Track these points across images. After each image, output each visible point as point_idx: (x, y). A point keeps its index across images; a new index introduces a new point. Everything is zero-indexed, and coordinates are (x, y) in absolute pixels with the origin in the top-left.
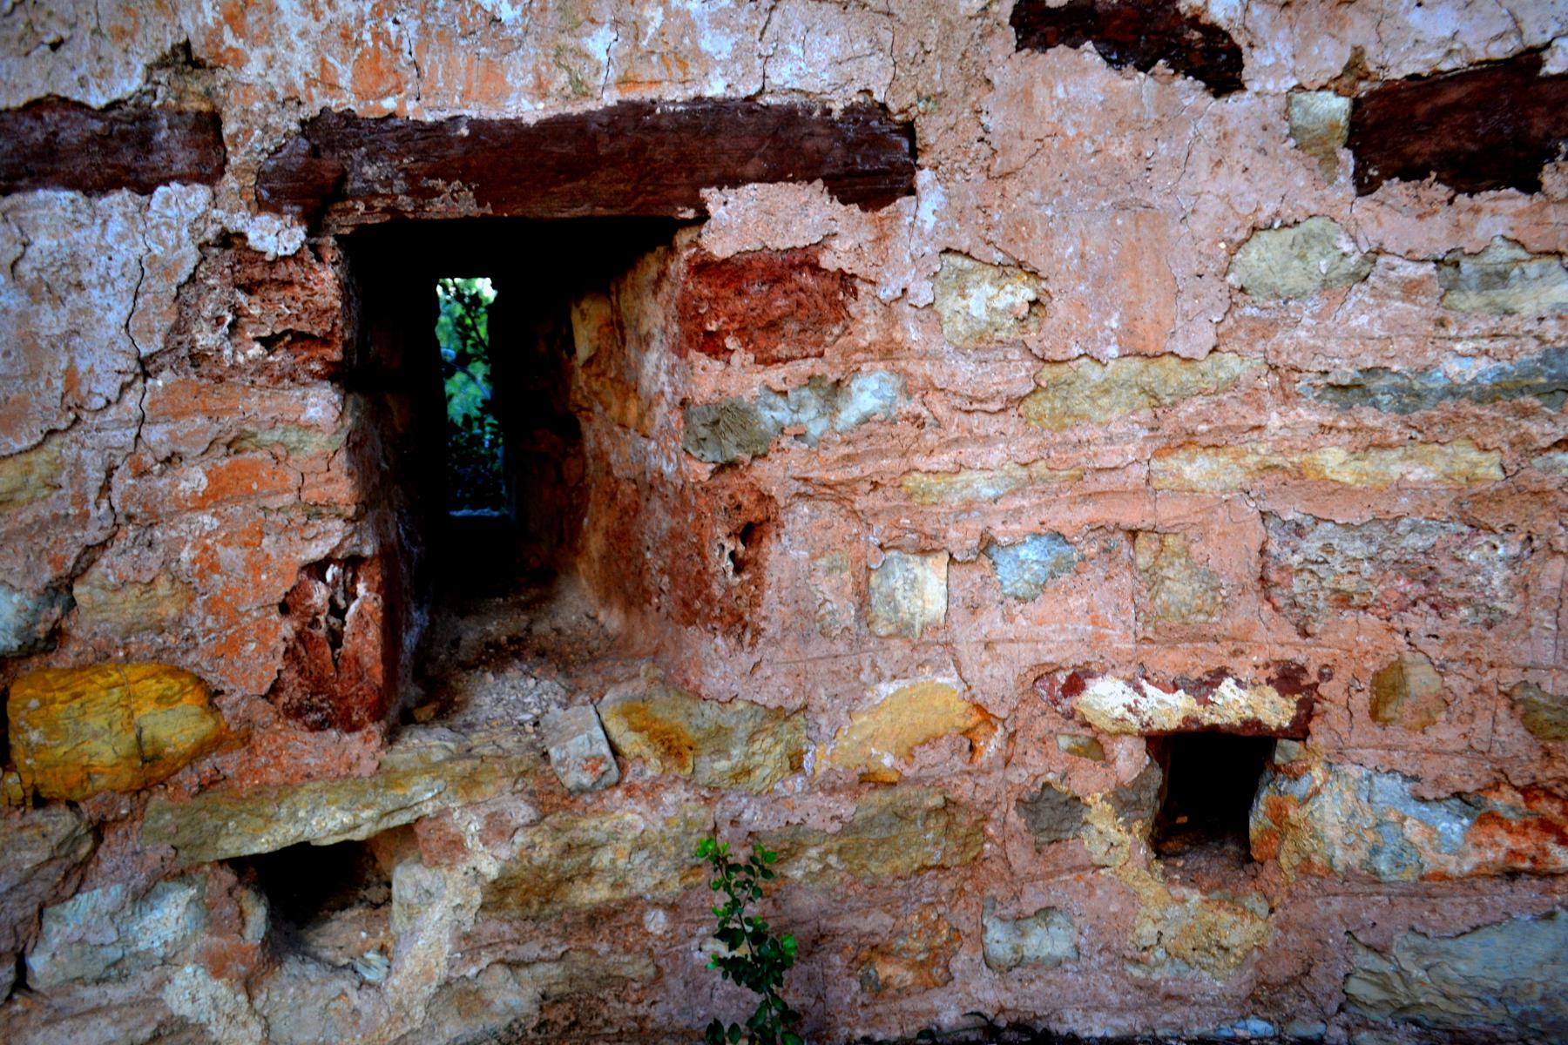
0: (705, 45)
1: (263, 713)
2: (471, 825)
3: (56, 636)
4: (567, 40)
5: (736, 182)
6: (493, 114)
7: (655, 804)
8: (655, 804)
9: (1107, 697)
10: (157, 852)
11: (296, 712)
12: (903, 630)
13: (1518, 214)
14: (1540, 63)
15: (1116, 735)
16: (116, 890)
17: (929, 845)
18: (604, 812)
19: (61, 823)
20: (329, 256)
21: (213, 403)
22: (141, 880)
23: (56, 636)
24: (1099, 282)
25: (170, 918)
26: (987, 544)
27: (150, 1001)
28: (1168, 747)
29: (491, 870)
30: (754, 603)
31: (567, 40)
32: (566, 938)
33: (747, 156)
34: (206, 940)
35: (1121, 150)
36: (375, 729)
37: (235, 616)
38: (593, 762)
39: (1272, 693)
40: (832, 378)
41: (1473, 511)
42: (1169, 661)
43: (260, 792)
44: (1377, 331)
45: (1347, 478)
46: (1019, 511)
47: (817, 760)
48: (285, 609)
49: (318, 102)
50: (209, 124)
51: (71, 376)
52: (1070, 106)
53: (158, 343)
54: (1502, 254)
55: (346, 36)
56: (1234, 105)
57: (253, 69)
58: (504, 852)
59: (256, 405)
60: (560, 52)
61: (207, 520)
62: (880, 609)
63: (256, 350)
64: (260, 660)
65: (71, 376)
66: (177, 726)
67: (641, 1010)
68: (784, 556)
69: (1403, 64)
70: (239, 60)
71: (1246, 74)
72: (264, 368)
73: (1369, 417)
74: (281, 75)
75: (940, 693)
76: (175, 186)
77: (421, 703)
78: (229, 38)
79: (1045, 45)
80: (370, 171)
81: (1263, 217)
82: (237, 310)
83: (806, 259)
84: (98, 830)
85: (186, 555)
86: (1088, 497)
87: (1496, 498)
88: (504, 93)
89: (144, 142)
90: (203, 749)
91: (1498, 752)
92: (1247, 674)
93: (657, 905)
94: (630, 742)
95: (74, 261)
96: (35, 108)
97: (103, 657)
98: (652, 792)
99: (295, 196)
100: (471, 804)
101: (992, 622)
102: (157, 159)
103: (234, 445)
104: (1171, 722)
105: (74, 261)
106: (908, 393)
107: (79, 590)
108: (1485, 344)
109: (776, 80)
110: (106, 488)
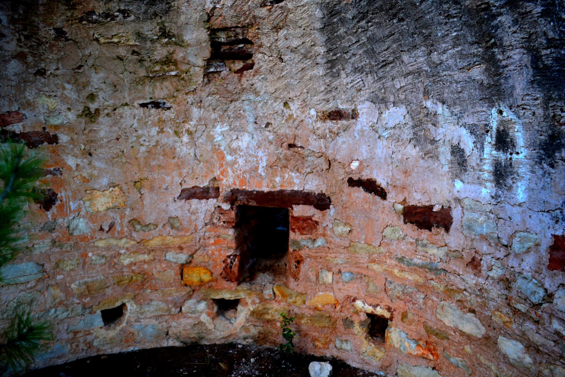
0: (295, 181)
1: (219, 277)
2: (249, 301)
3: (190, 262)
4: (272, 179)
5: (298, 204)
6: (260, 190)
7: (280, 304)
8: (280, 304)
9: (359, 304)
10: (202, 296)
11: (224, 278)
12: (324, 284)
13: (428, 235)
14: (432, 208)
15: (361, 311)
16: (195, 300)
17: (325, 323)
18: (270, 304)
19: (188, 289)
20: (234, 209)
21: (215, 230)
22: (199, 299)
23: (190, 262)
24: (362, 229)
25: (202, 306)
26: (340, 272)
27: (198, 318)
28: (371, 316)
29: (252, 309)
30: (298, 274)
31: (272, 179)
32: (263, 323)
33: (300, 200)
34: (207, 310)
35: (366, 206)
36: (236, 283)
37: (216, 262)
38: (270, 295)
39: (386, 311)
40: (313, 238)
41: (418, 287)
42: (370, 300)
43: (217, 289)
44: (405, 250)
45: (398, 275)
46: (346, 267)
47: (307, 303)
48: (224, 262)
49: (233, 187)
50: (218, 189)
51: (196, 225)
52: (358, 197)
53: (208, 221)
54: (425, 242)
55: (238, 177)
56: (385, 202)
57: (224, 181)
58: (254, 307)
59: (222, 231)
60: (271, 180)
61: (213, 247)
62: (321, 279)
63: (222, 223)
64: (219, 269)
65: (196, 225)
66: (206, 277)
67: (275, 339)
68: (304, 267)
69: (412, 203)
70: (222, 180)
71: (387, 197)
72: (223, 226)
73: (402, 265)
74: (228, 183)
75: (330, 297)
76: (212, 199)
77: (248, 277)
78: (221, 177)
79: (353, 186)
80: (241, 197)
81: (389, 224)
82: (220, 217)
83: (310, 218)
84: (194, 291)
85: (210, 252)
86: (358, 267)
87: (422, 286)
88: (262, 186)
89: (208, 192)
90: (210, 281)
91: (421, 333)
92: (382, 306)
93: (278, 321)
94: (277, 293)
95: (197, 209)
96: (193, 187)
97: (196, 266)
98: (279, 302)
99: (230, 201)
100: (249, 298)
101: (340, 285)
102: (210, 194)
103: (218, 237)
104: (370, 312)
105: (197, 209)
106: (327, 243)
107: (195, 256)
108: (422, 257)
109: (306, 188)
110: (199, 241)
